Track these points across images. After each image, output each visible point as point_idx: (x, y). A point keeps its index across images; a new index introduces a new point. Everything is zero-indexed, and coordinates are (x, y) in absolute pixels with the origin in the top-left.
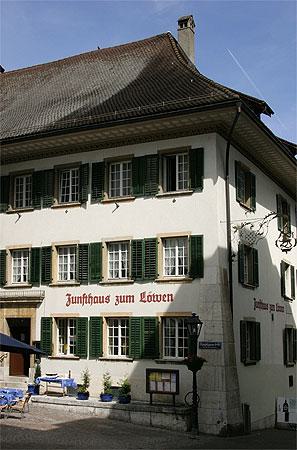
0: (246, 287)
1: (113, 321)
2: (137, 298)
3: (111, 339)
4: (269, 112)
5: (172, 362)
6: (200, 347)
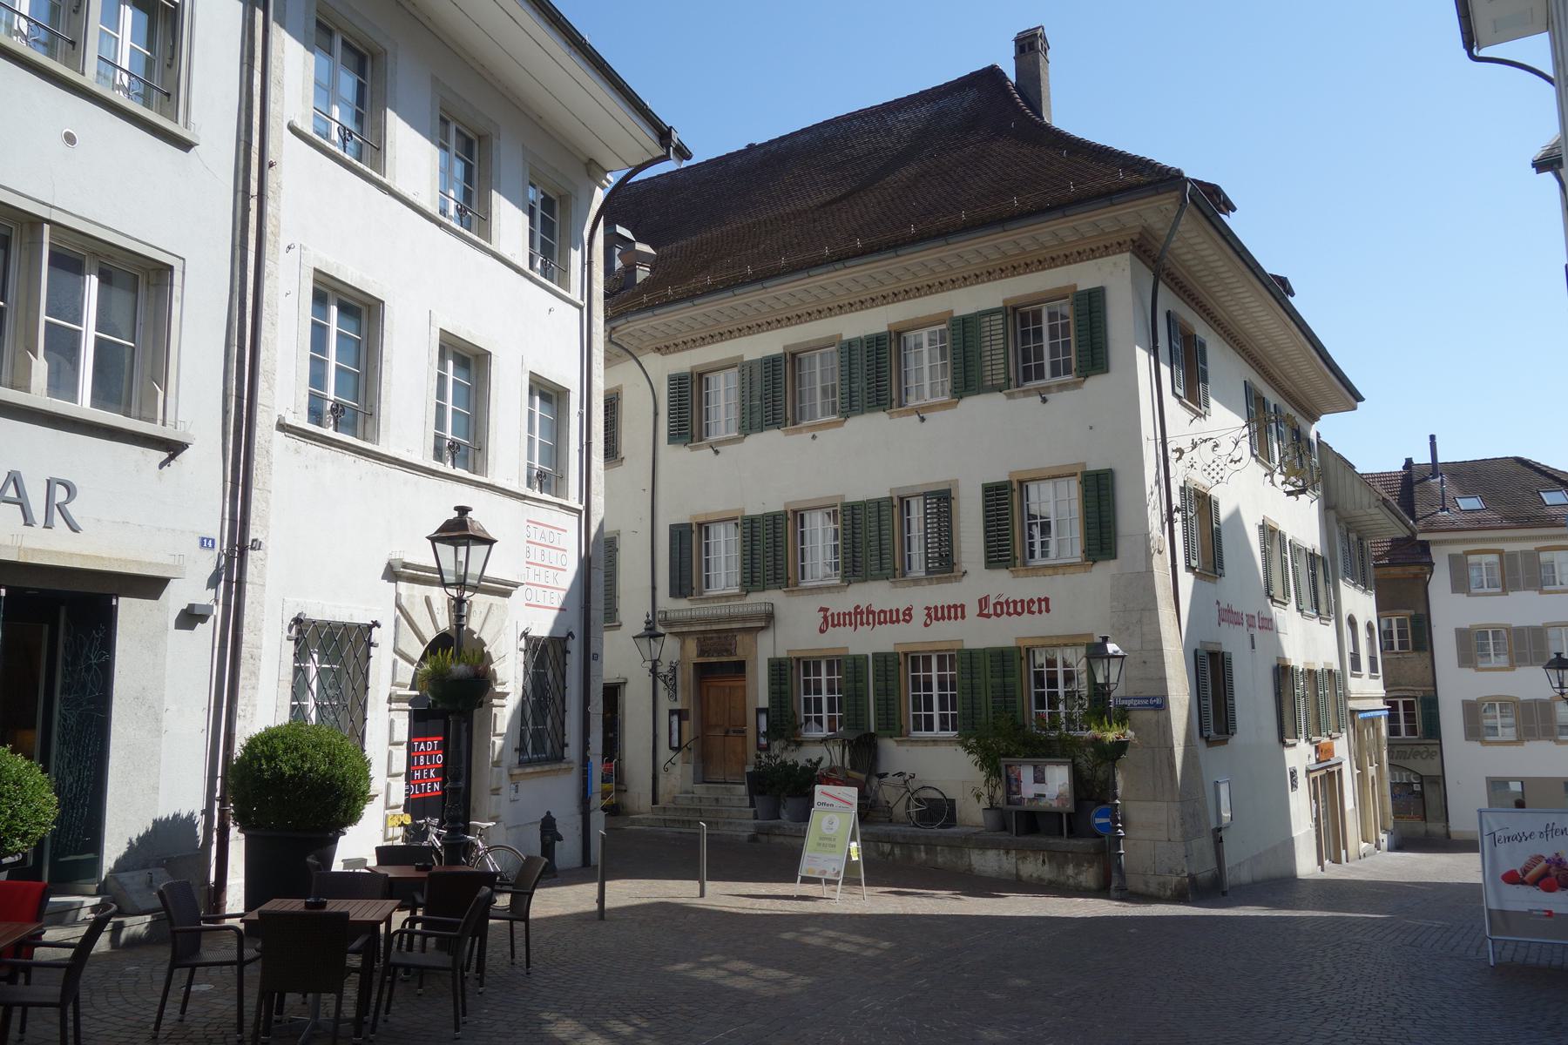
2: (972, 609)
6: (1475, 728)
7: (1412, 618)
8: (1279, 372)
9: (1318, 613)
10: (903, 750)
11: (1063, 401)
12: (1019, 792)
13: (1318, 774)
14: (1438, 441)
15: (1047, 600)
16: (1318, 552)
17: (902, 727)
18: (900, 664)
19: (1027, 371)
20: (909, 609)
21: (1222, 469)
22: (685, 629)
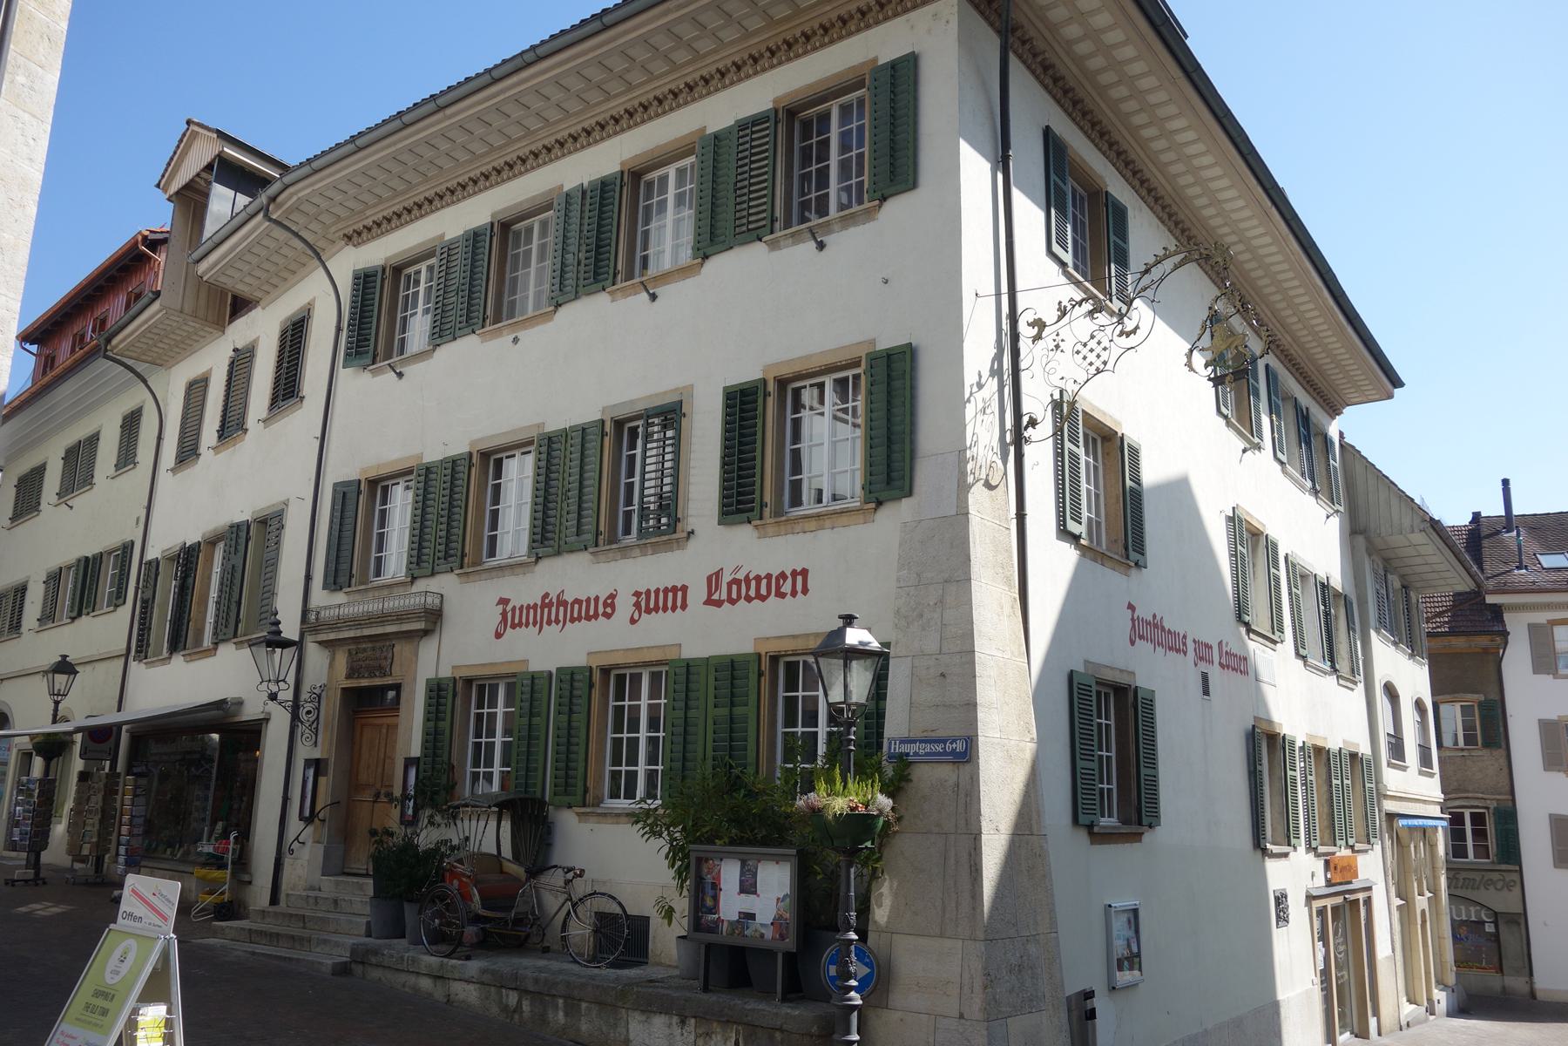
2: (697, 594)
7: (1480, 704)
8: (1269, 314)
9: (1333, 667)
10: (586, 827)
11: (848, 243)
12: (714, 909)
13: (1329, 903)
14: (1512, 486)
15: (804, 573)
16: (1337, 582)
17: (586, 791)
18: (591, 686)
19: (805, 206)
20: (612, 596)
21: (1105, 349)
22: (332, 636)
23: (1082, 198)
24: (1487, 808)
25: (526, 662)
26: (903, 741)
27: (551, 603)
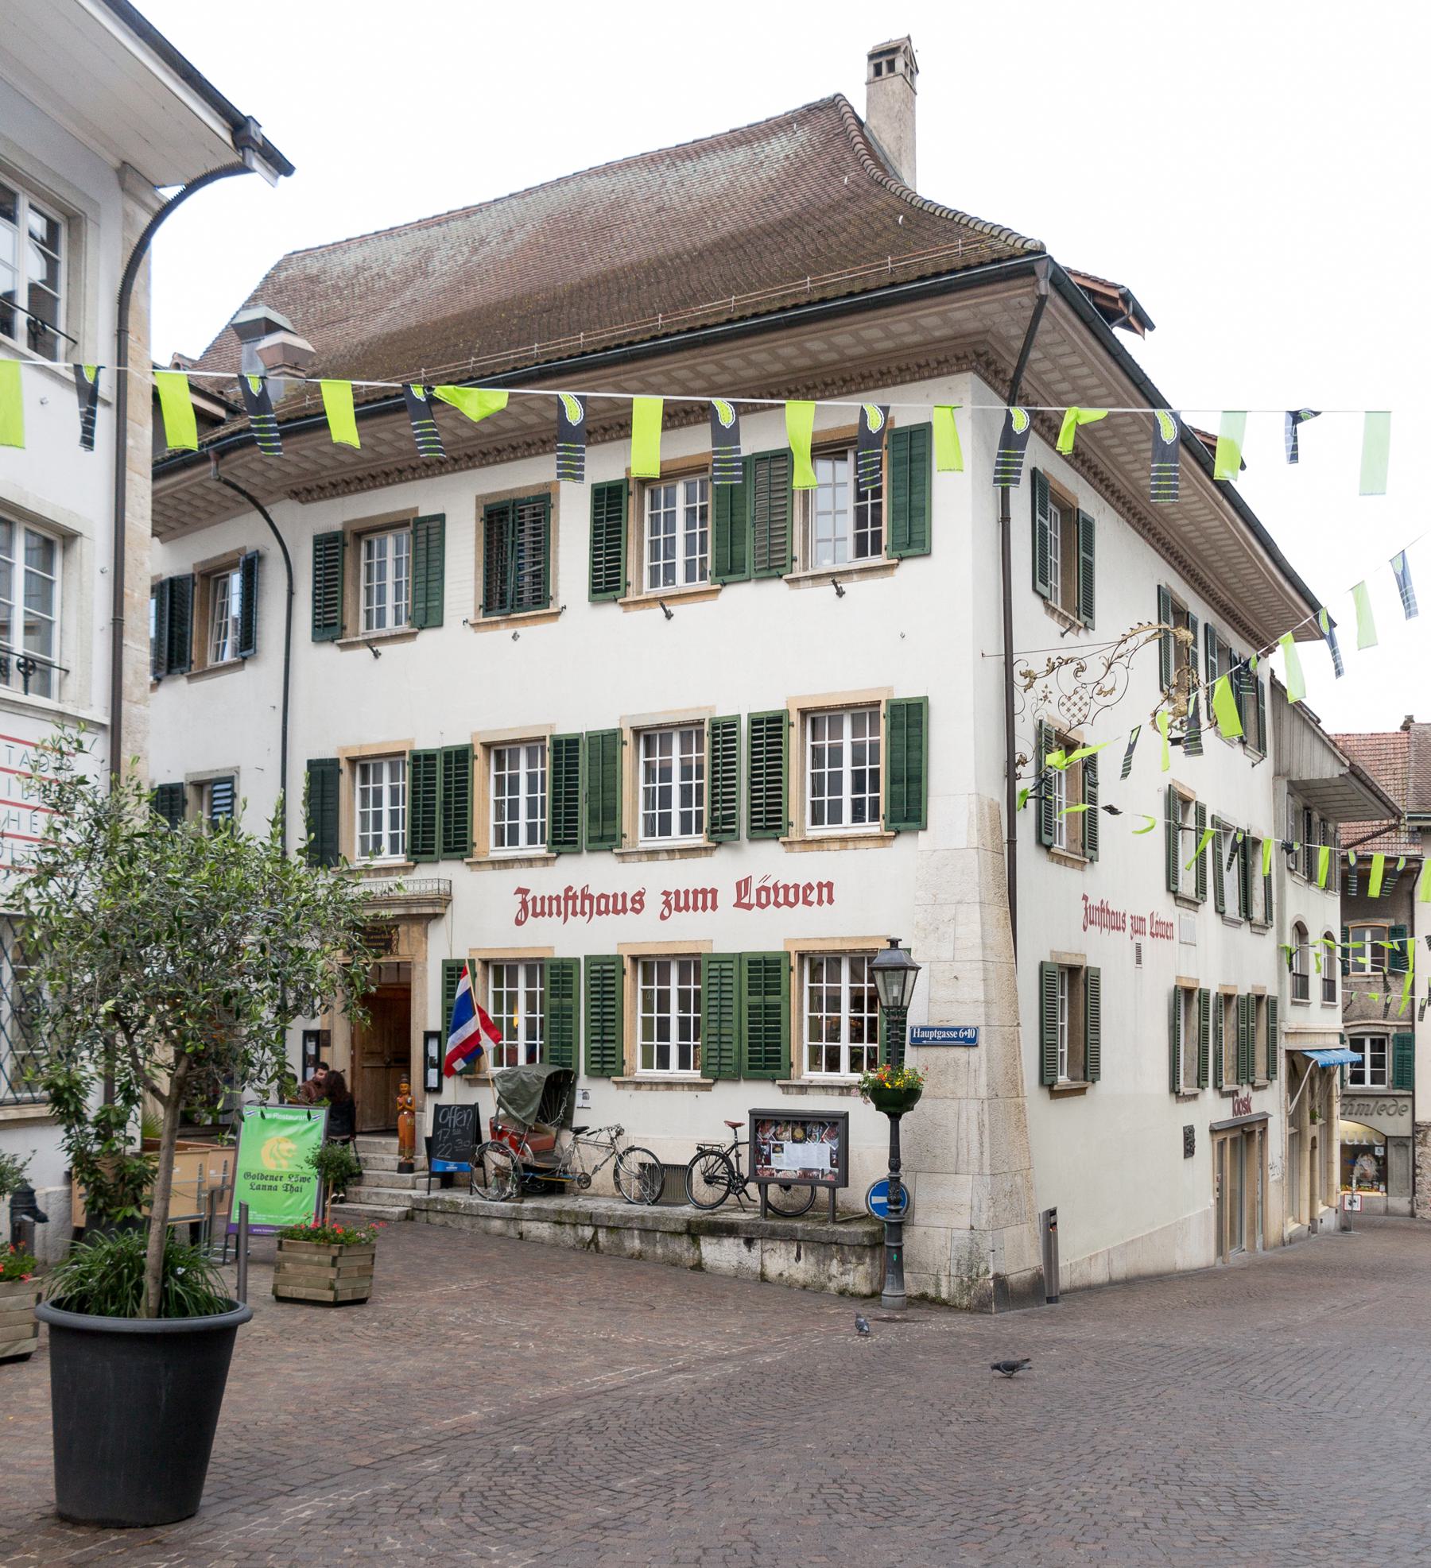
0: (1061, 859)
1: (652, 966)
3: (647, 1022)
4: (1142, 322)
5: (826, 1088)
15: (830, 885)
20: (640, 894)
21: (1086, 704)
23: (1055, 514)
24: (1387, 1034)
25: (551, 948)
26: (923, 1029)
27: (575, 897)
